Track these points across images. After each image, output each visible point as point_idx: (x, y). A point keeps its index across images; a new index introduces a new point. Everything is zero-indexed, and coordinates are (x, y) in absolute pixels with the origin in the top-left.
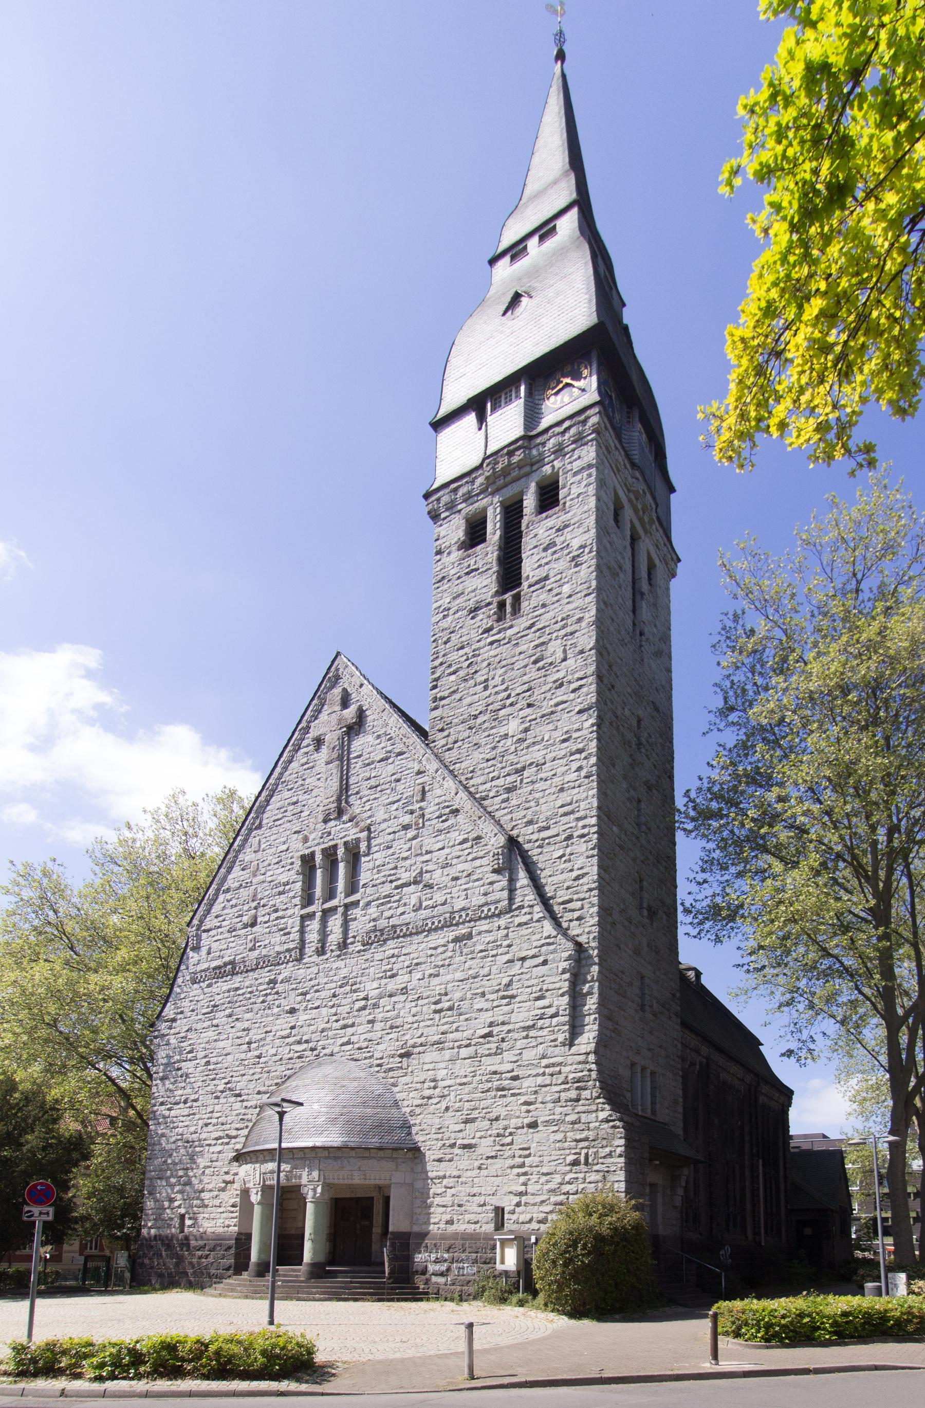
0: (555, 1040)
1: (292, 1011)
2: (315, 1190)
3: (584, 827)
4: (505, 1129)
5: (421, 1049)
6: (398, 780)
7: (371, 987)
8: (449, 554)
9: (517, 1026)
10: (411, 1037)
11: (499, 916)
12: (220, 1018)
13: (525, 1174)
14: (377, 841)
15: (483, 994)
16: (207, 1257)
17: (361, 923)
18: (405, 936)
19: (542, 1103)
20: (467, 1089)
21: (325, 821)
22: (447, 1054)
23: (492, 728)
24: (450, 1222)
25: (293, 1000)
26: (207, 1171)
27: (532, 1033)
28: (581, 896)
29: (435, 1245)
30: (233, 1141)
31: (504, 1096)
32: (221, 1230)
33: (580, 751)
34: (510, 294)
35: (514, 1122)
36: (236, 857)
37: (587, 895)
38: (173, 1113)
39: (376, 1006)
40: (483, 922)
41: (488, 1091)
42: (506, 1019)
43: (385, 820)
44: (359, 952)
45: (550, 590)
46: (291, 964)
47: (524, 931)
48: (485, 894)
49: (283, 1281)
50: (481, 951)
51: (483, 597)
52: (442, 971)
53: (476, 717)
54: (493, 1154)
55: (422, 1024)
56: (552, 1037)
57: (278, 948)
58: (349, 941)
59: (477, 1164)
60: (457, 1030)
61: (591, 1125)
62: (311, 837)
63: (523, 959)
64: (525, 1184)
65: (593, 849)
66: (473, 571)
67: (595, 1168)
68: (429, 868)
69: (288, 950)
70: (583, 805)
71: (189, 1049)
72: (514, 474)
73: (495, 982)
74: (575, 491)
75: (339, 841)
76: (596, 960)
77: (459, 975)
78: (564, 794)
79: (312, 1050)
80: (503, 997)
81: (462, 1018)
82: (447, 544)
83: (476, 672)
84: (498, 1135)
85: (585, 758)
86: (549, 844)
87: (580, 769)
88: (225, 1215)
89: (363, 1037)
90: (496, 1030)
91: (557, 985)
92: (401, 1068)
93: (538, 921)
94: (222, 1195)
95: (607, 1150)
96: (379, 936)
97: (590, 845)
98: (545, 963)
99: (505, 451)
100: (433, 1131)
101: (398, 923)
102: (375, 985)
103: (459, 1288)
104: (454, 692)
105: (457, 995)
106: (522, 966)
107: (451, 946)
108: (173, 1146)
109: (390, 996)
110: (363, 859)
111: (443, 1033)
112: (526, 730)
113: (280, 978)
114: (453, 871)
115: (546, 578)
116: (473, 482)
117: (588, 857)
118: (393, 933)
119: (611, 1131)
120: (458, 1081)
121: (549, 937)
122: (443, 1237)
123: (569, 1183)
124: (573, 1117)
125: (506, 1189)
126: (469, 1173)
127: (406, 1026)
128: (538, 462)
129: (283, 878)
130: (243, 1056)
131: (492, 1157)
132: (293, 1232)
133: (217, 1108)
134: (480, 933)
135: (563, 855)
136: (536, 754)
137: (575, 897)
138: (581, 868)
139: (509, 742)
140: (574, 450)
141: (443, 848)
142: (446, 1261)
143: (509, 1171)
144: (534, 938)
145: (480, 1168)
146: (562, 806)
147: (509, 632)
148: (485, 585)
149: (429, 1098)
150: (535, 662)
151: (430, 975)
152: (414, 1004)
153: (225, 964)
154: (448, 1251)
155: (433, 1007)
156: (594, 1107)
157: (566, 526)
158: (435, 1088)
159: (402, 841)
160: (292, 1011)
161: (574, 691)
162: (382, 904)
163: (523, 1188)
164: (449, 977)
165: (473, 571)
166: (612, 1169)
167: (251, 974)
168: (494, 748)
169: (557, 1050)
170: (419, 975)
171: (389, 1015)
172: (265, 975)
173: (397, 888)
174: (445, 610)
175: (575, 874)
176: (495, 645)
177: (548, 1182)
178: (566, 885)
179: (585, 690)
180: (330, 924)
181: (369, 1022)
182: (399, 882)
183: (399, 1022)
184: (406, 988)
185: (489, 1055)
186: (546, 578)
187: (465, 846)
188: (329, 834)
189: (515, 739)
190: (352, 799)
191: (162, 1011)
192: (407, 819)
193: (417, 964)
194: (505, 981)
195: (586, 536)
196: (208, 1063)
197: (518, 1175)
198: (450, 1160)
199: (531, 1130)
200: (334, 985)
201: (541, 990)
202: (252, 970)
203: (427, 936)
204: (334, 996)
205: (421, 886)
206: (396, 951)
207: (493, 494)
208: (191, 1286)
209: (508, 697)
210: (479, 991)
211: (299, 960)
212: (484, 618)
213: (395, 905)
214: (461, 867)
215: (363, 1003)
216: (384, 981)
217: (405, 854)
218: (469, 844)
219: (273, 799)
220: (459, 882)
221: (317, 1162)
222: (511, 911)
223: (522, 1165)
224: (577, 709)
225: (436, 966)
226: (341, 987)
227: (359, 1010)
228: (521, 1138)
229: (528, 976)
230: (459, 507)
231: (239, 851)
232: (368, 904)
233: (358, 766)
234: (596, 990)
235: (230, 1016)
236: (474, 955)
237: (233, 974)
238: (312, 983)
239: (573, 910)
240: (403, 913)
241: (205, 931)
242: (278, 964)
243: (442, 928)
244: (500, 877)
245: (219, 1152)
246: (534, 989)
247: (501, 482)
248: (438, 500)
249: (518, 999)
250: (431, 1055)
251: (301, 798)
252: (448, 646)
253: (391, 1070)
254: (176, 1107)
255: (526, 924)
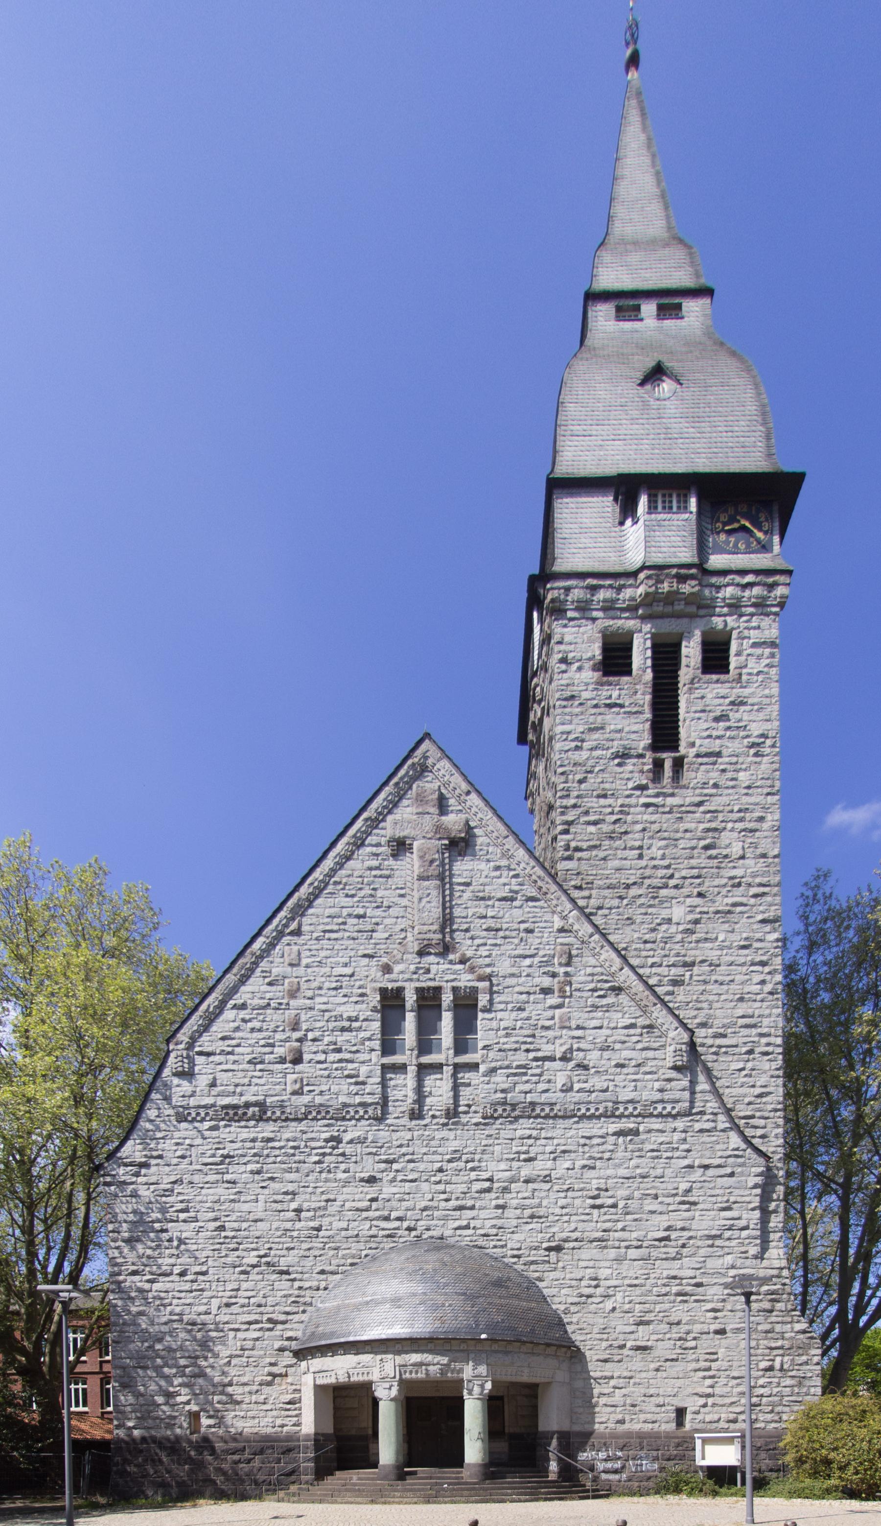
0: (746, 1252)
1: (372, 1180)
2: (482, 1386)
3: (768, 1044)
4: (688, 1333)
5: (576, 1244)
6: (530, 931)
7: (498, 1169)
8: (580, 669)
9: (700, 1233)
10: (560, 1230)
11: (674, 1117)
12: (239, 1172)
13: (713, 1377)
14: (502, 998)
15: (656, 1197)
16: (249, 1461)
17: (479, 1089)
18: (547, 1117)
19: (732, 1311)
20: (638, 1291)
21: (421, 953)
22: (612, 1253)
23: (650, 906)
24: (622, 1422)
25: (369, 1167)
26: (234, 1361)
27: (718, 1242)
28: (766, 1114)
29: (605, 1444)
30: (280, 1327)
31: (686, 1301)
32: (269, 1430)
33: (763, 964)
34: (650, 364)
35: (697, 1328)
36: (256, 964)
37: (772, 1114)
38: (156, 1286)
39: (506, 1190)
40: (654, 1120)
41: (665, 1295)
42: (687, 1224)
43: (513, 975)
44: (476, 1124)
45: (724, 771)
46: (363, 1122)
47: (705, 1138)
48: (661, 1091)
49: (449, 1484)
50: (653, 1151)
51: (634, 744)
52: (598, 1164)
53: (628, 887)
54: (675, 1357)
55: (574, 1218)
56: (743, 1249)
57: (342, 1099)
58: (461, 1109)
59: (653, 1366)
60: (623, 1230)
61: (786, 1335)
62: (397, 968)
63: (706, 1167)
64: (712, 1387)
65: (777, 1069)
66: (616, 705)
67: (790, 1374)
68: (583, 1046)
69: (363, 1105)
70: (766, 1022)
71: (180, 1206)
72: (679, 607)
73: (670, 1186)
74: (753, 666)
75: (444, 984)
76: (782, 1180)
77: (622, 1172)
78: (744, 1005)
79: (409, 1229)
80: (683, 1203)
81: (629, 1217)
82: (578, 655)
83: (626, 833)
84: (680, 1339)
85: (769, 973)
86: (726, 1053)
87: (763, 982)
88: (274, 1413)
89: (488, 1223)
90: (674, 1235)
91: (747, 1199)
92: (549, 1262)
93: (723, 1131)
94: (266, 1390)
95: (804, 1358)
96: (507, 1111)
97: (774, 1065)
98: (732, 1175)
99: (674, 571)
100: (596, 1330)
101: (538, 1100)
102: (503, 1166)
103: (637, 1484)
104: (595, 847)
105: (622, 1193)
106: (703, 1175)
107: (611, 1139)
108: (165, 1329)
109: (527, 1181)
110: (480, 1015)
111: (605, 1231)
112: (697, 922)
113: (347, 1137)
114: (617, 1058)
115: (718, 754)
116: (619, 589)
117: (772, 1077)
118: (531, 1111)
119: (807, 1341)
120: (627, 1282)
121: (737, 1149)
122: (614, 1436)
123: (762, 1386)
124: (767, 1327)
125: (690, 1390)
126: (644, 1375)
127: (551, 1218)
128: (708, 607)
129: (349, 1010)
130: (289, 1225)
131: (672, 1360)
132: (353, 1432)
133: (244, 1285)
134: (649, 1131)
135: (743, 1069)
136: (709, 952)
137: (758, 1114)
138: (765, 1086)
139: (673, 929)
140: (752, 615)
141: (601, 1028)
142: (619, 1458)
143: (692, 1374)
144: (718, 1147)
145: (657, 1370)
146: (743, 1017)
147: (670, 801)
148: (638, 731)
149: (589, 1296)
150: (706, 848)
151: (584, 1167)
152: (563, 1195)
153: (247, 1105)
154: (622, 1450)
155: (590, 1202)
156: (790, 1319)
157: (742, 703)
158: (596, 1286)
159: (540, 1006)
160: (372, 1180)
161: (755, 896)
162: (515, 1075)
163: (710, 1390)
164: (609, 1172)
165: (616, 705)
166: (809, 1375)
167: (294, 1124)
168: (653, 930)
169: (748, 1262)
170: (568, 1164)
171: (527, 1202)
172: (321, 1131)
173: (536, 1059)
174: (576, 739)
175: (758, 1091)
176: (651, 809)
177: (738, 1385)
178: (747, 1100)
179: (769, 899)
180: (427, 1083)
181: (498, 1207)
182: (540, 1054)
183: (542, 1212)
184: (550, 1175)
185: (666, 1259)
186: (718, 754)
187: (632, 1031)
188: (428, 971)
189: (681, 928)
190: (458, 936)
191: (118, 1149)
192: (547, 982)
193: (564, 1152)
194: (684, 1186)
195: (768, 726)
196: (222, 1228)
197: (704, 1378)
198: (619, 1361)
199: (719, 1336)
200: (439, 1158)
201: (727, 1201)
202: (296, 1119)
203: (577, 1122)
204: (441, 1170)
205: (572, 1064)
206: (534, 1133)
207: (643, 618)
208: (220, 1495)
209: (672, 877)
210: (653, 1192)
211: (380, 1119)
212: (635, 771)
213: (535, 1079)
214: (626, 1054)
215: (487, 1184)
216: (515, 1164)
217: (548, 1023)
218: (638, 1031)
219: (319, 901)
220: (625, 1070)
221: (484, 1355)
222: (690, 1114)
223: (709, 1369)
224: (760, 917)
225: (591, 1158)
226: (449, 1161)
227: (481, 1192)
228: (706, 1344)
229: (712, 1185)
230: (595, 614)
231: (261, 957)
232: (493, 1070)
233: (467, 895)
234: (781, 1209)
235: (258, 1172)
236: (643, 1154)
237: (261, 1119)
238: (404, 1150)
239: (756, 1127)
240: (546, 1091)
241: (200, 1053)
242: (344, 1119)
243: (599, 1117)
244: (680, 1076)
245: (257, 1339)
246: (719, 1199)
247: (659, 608)
248: (568, 590)
249: (700, 1207)
250: (588, 1252)
251: (369, 912)
252: (583, 786)
253: (533, 1263)
254: (161, 1278)
255: (708, 1131)
